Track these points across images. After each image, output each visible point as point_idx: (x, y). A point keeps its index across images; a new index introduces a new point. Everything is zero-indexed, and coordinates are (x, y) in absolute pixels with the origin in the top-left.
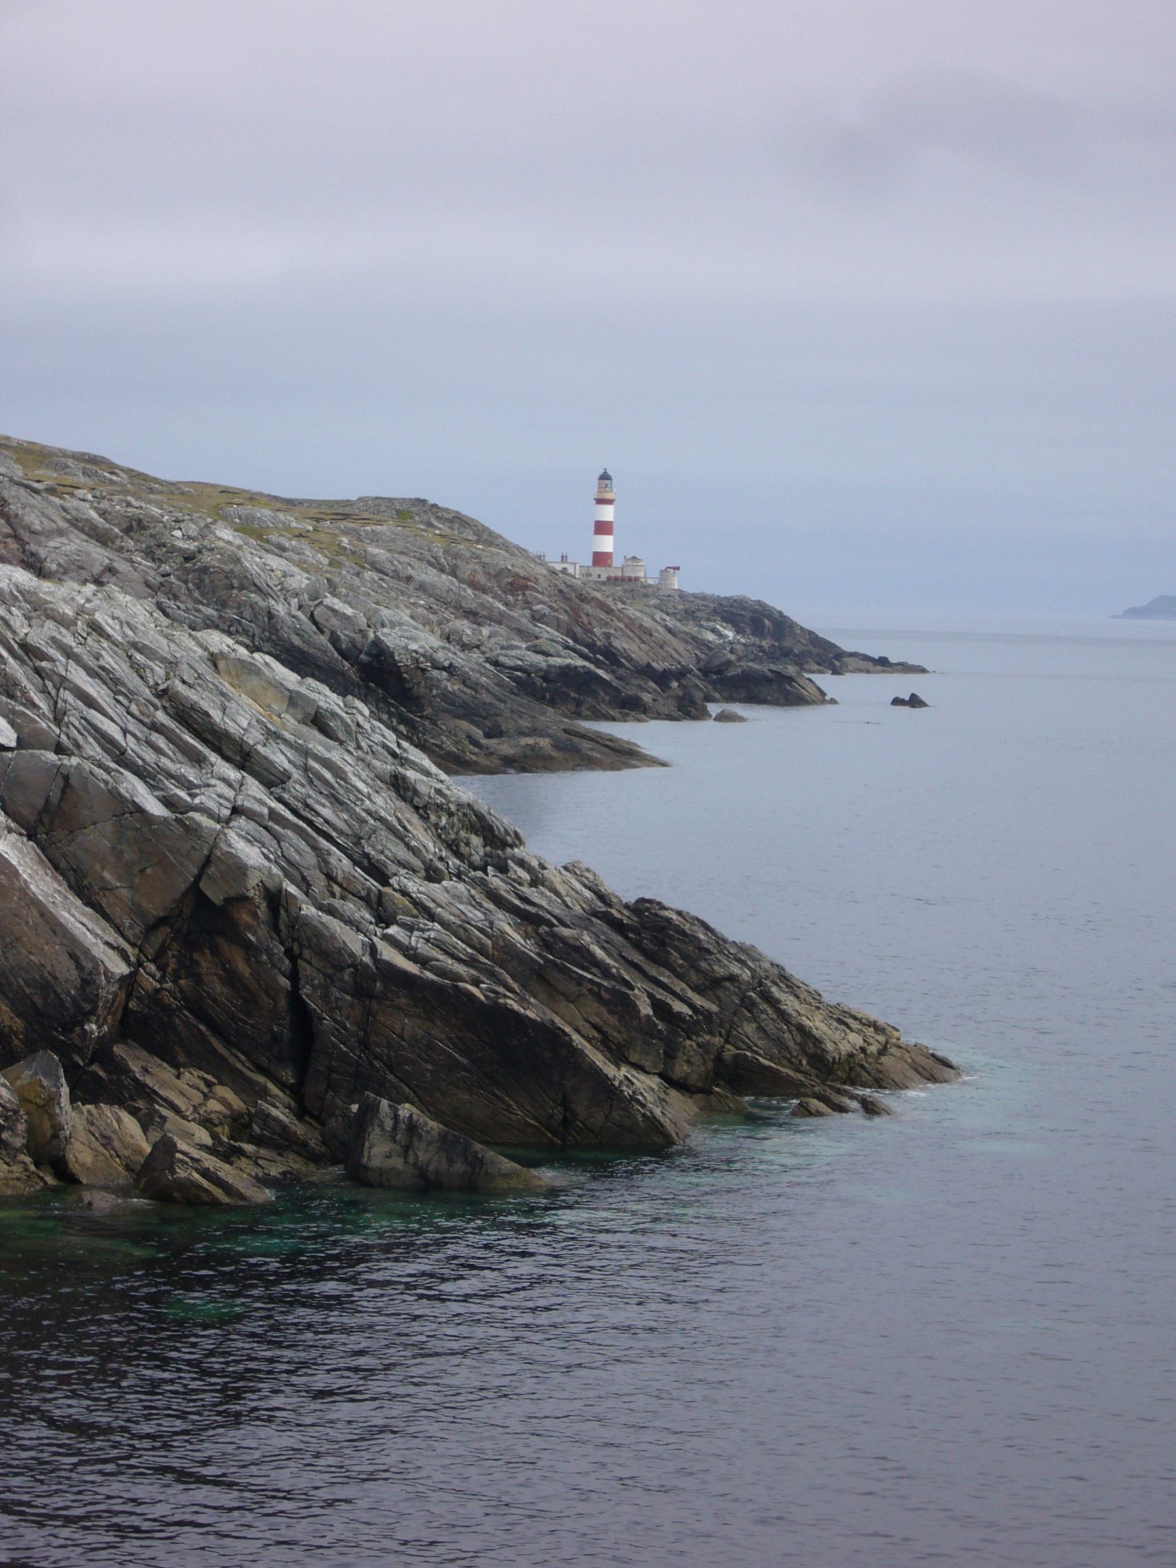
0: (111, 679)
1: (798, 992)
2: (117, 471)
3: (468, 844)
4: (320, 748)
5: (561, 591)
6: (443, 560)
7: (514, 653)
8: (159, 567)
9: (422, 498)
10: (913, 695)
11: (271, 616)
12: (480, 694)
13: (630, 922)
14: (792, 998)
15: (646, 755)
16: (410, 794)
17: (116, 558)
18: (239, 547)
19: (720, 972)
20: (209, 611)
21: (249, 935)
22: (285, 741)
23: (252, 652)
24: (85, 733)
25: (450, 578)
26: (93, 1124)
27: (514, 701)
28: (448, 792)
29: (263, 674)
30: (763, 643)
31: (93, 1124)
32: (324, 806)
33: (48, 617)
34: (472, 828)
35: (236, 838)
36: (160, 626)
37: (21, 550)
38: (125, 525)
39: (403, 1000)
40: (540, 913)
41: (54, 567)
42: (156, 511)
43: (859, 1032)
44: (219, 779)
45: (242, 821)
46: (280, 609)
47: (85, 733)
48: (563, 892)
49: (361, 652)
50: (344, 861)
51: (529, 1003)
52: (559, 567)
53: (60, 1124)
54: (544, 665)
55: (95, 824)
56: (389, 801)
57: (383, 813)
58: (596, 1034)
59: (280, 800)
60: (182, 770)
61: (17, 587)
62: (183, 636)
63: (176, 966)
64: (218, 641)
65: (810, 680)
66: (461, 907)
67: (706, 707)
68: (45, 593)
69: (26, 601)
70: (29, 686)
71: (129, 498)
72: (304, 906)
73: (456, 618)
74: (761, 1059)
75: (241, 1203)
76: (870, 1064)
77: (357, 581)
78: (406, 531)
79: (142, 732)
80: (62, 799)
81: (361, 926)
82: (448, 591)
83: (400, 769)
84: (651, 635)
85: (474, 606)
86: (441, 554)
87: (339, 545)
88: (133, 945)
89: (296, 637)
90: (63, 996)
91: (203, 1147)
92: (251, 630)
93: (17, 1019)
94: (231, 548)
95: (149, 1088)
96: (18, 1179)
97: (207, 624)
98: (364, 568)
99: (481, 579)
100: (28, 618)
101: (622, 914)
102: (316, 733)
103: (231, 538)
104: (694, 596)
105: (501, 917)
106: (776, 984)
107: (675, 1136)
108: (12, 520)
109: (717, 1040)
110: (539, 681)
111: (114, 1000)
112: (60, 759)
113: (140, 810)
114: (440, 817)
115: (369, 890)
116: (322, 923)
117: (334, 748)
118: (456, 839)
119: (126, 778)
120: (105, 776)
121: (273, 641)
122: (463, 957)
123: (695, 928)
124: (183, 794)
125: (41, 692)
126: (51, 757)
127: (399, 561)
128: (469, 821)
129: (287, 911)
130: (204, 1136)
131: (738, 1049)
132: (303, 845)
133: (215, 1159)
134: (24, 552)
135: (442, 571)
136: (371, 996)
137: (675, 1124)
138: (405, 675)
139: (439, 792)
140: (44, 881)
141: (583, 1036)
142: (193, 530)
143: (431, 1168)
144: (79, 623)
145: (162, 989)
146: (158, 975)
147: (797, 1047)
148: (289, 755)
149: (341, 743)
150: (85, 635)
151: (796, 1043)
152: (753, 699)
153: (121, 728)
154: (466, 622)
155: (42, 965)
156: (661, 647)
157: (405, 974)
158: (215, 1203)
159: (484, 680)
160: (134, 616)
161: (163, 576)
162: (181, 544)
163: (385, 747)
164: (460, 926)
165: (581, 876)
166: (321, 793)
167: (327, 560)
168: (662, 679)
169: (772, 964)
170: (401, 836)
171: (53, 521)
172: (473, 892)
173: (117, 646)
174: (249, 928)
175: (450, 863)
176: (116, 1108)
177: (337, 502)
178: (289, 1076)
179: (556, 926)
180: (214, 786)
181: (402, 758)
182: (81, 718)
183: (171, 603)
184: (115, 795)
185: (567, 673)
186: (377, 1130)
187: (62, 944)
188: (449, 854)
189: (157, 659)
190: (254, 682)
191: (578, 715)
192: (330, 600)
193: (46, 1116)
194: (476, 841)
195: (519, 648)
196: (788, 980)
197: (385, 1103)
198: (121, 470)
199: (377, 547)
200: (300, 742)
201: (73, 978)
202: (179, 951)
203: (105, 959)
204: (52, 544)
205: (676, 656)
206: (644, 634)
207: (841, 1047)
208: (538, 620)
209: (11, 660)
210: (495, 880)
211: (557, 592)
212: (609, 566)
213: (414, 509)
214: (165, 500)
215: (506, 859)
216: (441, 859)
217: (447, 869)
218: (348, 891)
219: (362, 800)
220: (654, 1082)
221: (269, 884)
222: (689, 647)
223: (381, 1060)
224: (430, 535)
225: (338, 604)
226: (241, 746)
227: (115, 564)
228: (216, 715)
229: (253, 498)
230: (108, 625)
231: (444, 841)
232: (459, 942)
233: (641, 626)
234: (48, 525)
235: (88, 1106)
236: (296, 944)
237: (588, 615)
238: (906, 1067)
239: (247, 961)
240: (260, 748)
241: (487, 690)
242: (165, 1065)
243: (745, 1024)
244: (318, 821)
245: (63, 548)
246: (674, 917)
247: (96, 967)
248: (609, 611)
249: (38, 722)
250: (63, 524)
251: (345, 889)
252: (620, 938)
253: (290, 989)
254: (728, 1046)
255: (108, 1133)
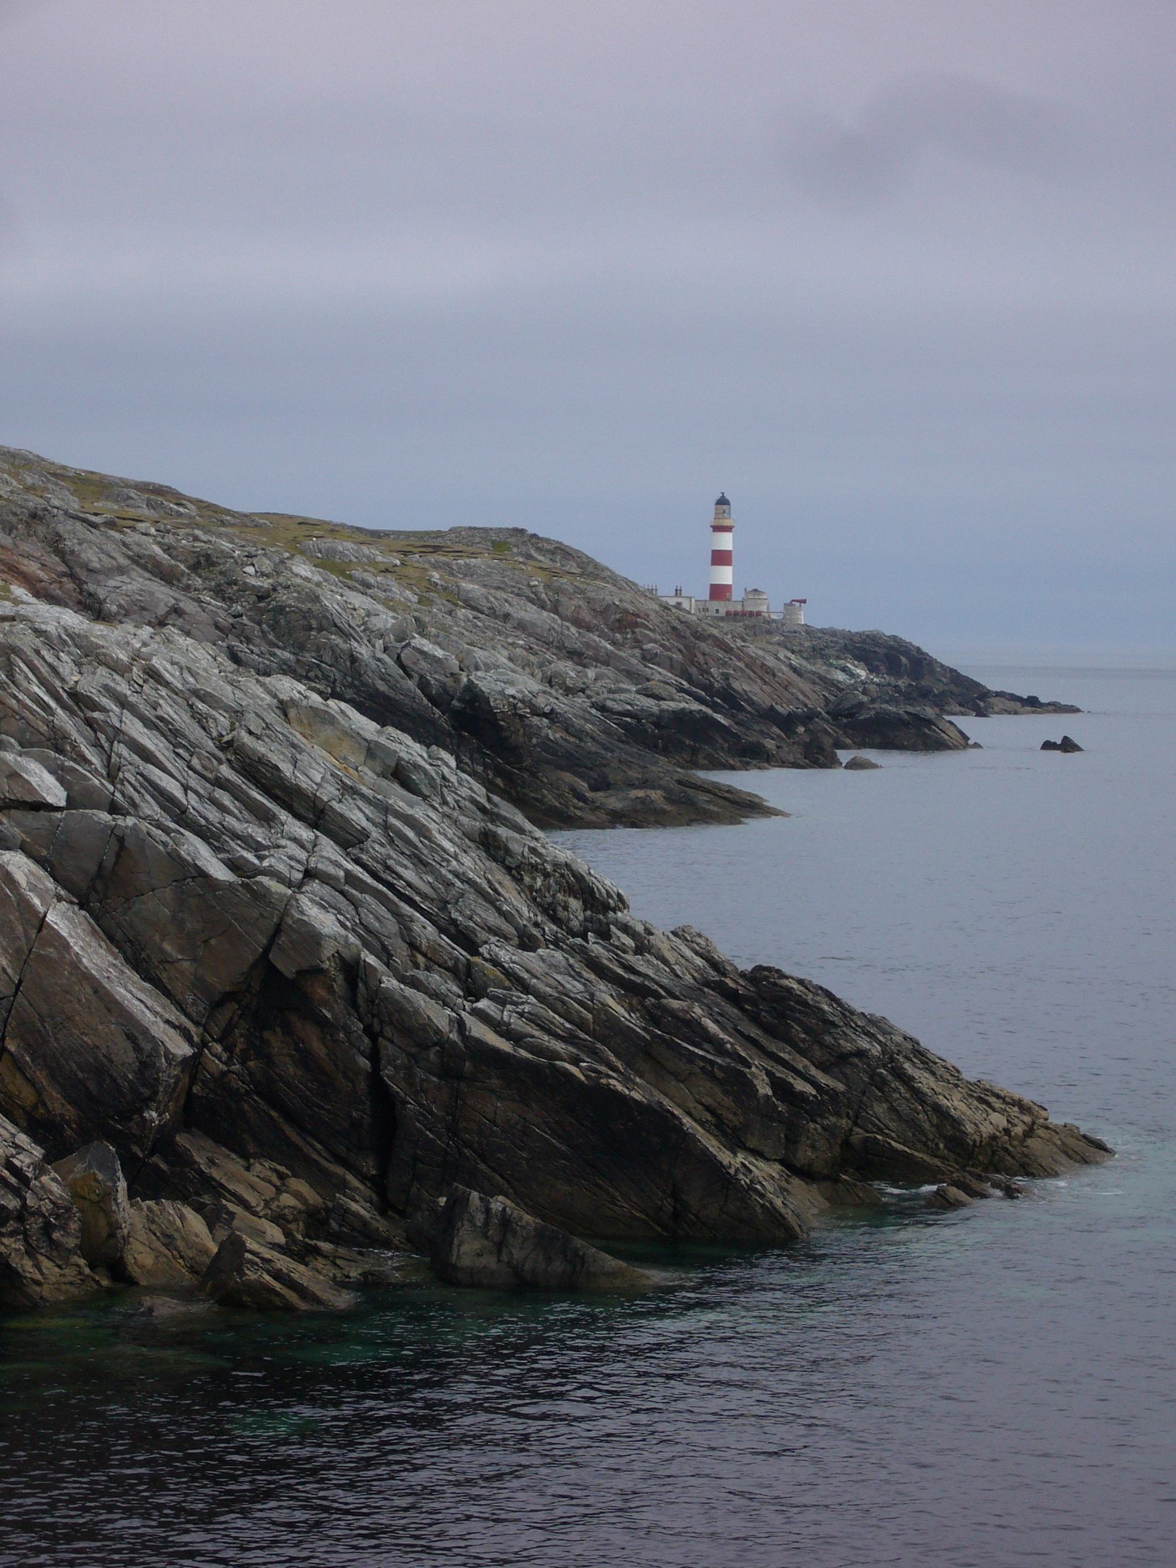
0: (170, 730)
1: (934, 1068)
2: (185, 502)
3: (566, 908)
4: (401, 804)
5: (674, 628)
6: (544, 596)
7: (623, 696)
8: (230, 607)
9: (520, 527)
10: (1065, 738)
11: (353, 659)
12: (586, 742)
13: (747, 993)
14: (927, 1075)
15: (768, 808)
16: (501, 853)
17: (183, 598)
18: (318, 584)
19: (848, 1046)
20: (286, 655)
21: (324, 1011)
22: (363, 797)
23: (326, 699)
24: (142, 791)
25: (552, 615)
26: (153, 1222)
27: (622, 749)
28: (543, 851)
29: (339, 723)
30: (900, 683)
31: (153, 1222)
32: (406, 867)
33: (101, 663)
34: (571, 891)
35: (310, 904)
36: (225, 671)
37: (78, 590)
38: (191, 562)
39: (495, 1081)
40: (646, 983)
41: (114, 608)
42: (226, 545)
43: (1002, 1112)
44: (290, 839)
45: (315, 885)
46: (363, 651)
47: (142, 791)
48: (672, 960)
49: (453, 698)
50: (429, 929)
51: (635, 1083)
52: (672, 602)
53: (117, 1221)
54: (655, 710)
55: (153, 890)
56: (478, 861)
57: (471, 875)
58: (709, 1117)
59: (358, 861)
60: (250, 830)
61: (66, 630)
62: (249, 682)
63: (245, 1047)
64: (289, 687)
65: (950, 722)
66: (559, 977)
67: (835, 754)
68: (97, 637)
69: (76, 646)
70: (80, 739)
71: (197, 532)
72: (384, 979)
73: (559, 659)
74: (893, 1143)
75: (315, 1307)
76: (1014, 1147)
77: (449, 620)
78: (503, 564)
79: (205, 789)
80: (116, 863)
81: (448, 1000)
82: (549, 630)
83: (490, 826)
84: (774, 675)
85: (578, 645)
86: (541, 589)
87: (429, 580)
88: (197, 1023)
89: (381, 682)
90: (119, 1081)
91: (275, 1246)
92: (331, 675)
93: (69, 1107)
94: (309, 585)
95: (215, 1180)
96: (71, 1283)
97: (282, 669)
98: (456, 605)
99: (586, 616)
100: (78, 664)
101: (737, 983)
102: (396, 787)
103: (309, 575)
104: (822, 631)
105: (603, 987)
106: (910, 1060)
107: (797, 1229)
108: (68, 557)
109: (844, 1123)
110: (650, 728)
111: (176, 1084)
112: (114, 819)
113: (203, 874)
114: (534, 879)
115: (457, 959)
116: (405, 997)
117: (417, 804)
118: (553, 903)
119: (187, 839)
120: (164, 838)
121: (356, 687)
122: (560, 1032)
123: (818, 998)
124: (250, 856)
125: (93, 746)
126: (105, 817)
127: (494, 597)
128: (567, 882)
129: (365, 984)
130: (276, 1234)
131: (867, 1132)
132: (382, 911)
133: (288, 1259)
134: (81, 592)
135: (543, 607)
136: (460, 1077)
137: (798, 1216)
138: (502, 723)
139: (533, 850)
140: (97, 953)
141: (695, 1120)
142: (267, 565)
143: (527, 1267)
144: (135, 669)
145: (230, 1071)
146: (225, 1056)
147: (933, 1129)
148: (367, 811)
149: (425, 798)
150: (141, 682)
151: (932, 1125)
152: (887, 745)
153: (182, 785)
154: (569, 664)
155: (97, 1047)
156: (786, 688)
157: (496, 1051)
158: (289, 1308)
159: (589, 726)
160: (196, 660)
161: (235, 617)
162: (253, 582)
163: (474, 801)
164: (557, 999)
165: (692, 942)
166: (403, 853)
167: (416, 597)
168: (787, 723)
169: (905, 1038)
170: (491, 899)
171: (112, 558)
172: (571, 961)
173: (177, 694)
174: (325, 1003)
175: (546, 929)
176: (179, 1205)
177: (427, 533)
178: (369, 1166)
179: (664, 997)
180: (284, 847)
181: (493, 814)
182: (138, 773)
183: (243, 647)
184: (175, 858)
185: (681, 717)
186: (467, 1225)
187: (118, 1024)
188: (545, 919)
189: (220, 708)
190: (328, 732)
191: (697, 766)
192: (419, 641)
193: (101, 1214)
194: (575, 904)
195: (629, 691)
196: (923, 1055)
197: (475, 1195)
198: (189, 501)
199: (472, 582)
200: (379, 797)
201: (131, 1061)
202: (248, 1030)
203: (165, 1039)
204: (112, 583)
205: (801, 697)
206: (766, 673)
207: (983, 1129)
208: (649, 661)
209: (59, 711)
210: (596, 948)
211: (669, 629)
212: (729, 600)
213: (513, 540)
214: (237, 533)
215: (608, 924)
216: (536, 925)
217: (543, 936)
218: (434, 961)
219: (448, 861)
220: (775, 1169)
221: (346, 954)
222: (817, 688)
223: (471, 1147)
224: (530, 568)
225: (427, 646)
226: (314, 803)
227: (181, 605)
228: (286, 769)
229: (334, 530)
230: (167, 671)
231: (539, 905)
232: (556, 1016)
233: (763, 665)
234: (107, 561)
235: (148, 1202)
236: (376, 1020)
237: (704, 654)
238: (1055, 1150)
239: (322, 1040)
240: (334, 804)
241: (593, 738)
242: (233, 1156)
243: (875, 1104)
244: (401, 884)
245: (124, 588)
246: (795, 986)
247: (156, 1048)
248: (728, 649)
249: (90, 779)
250: (124, 562)
251: (430, 959)
252: (736, 1011)
253: (370, 1070)
254: (856, 1129)
255: (170, 1231)
